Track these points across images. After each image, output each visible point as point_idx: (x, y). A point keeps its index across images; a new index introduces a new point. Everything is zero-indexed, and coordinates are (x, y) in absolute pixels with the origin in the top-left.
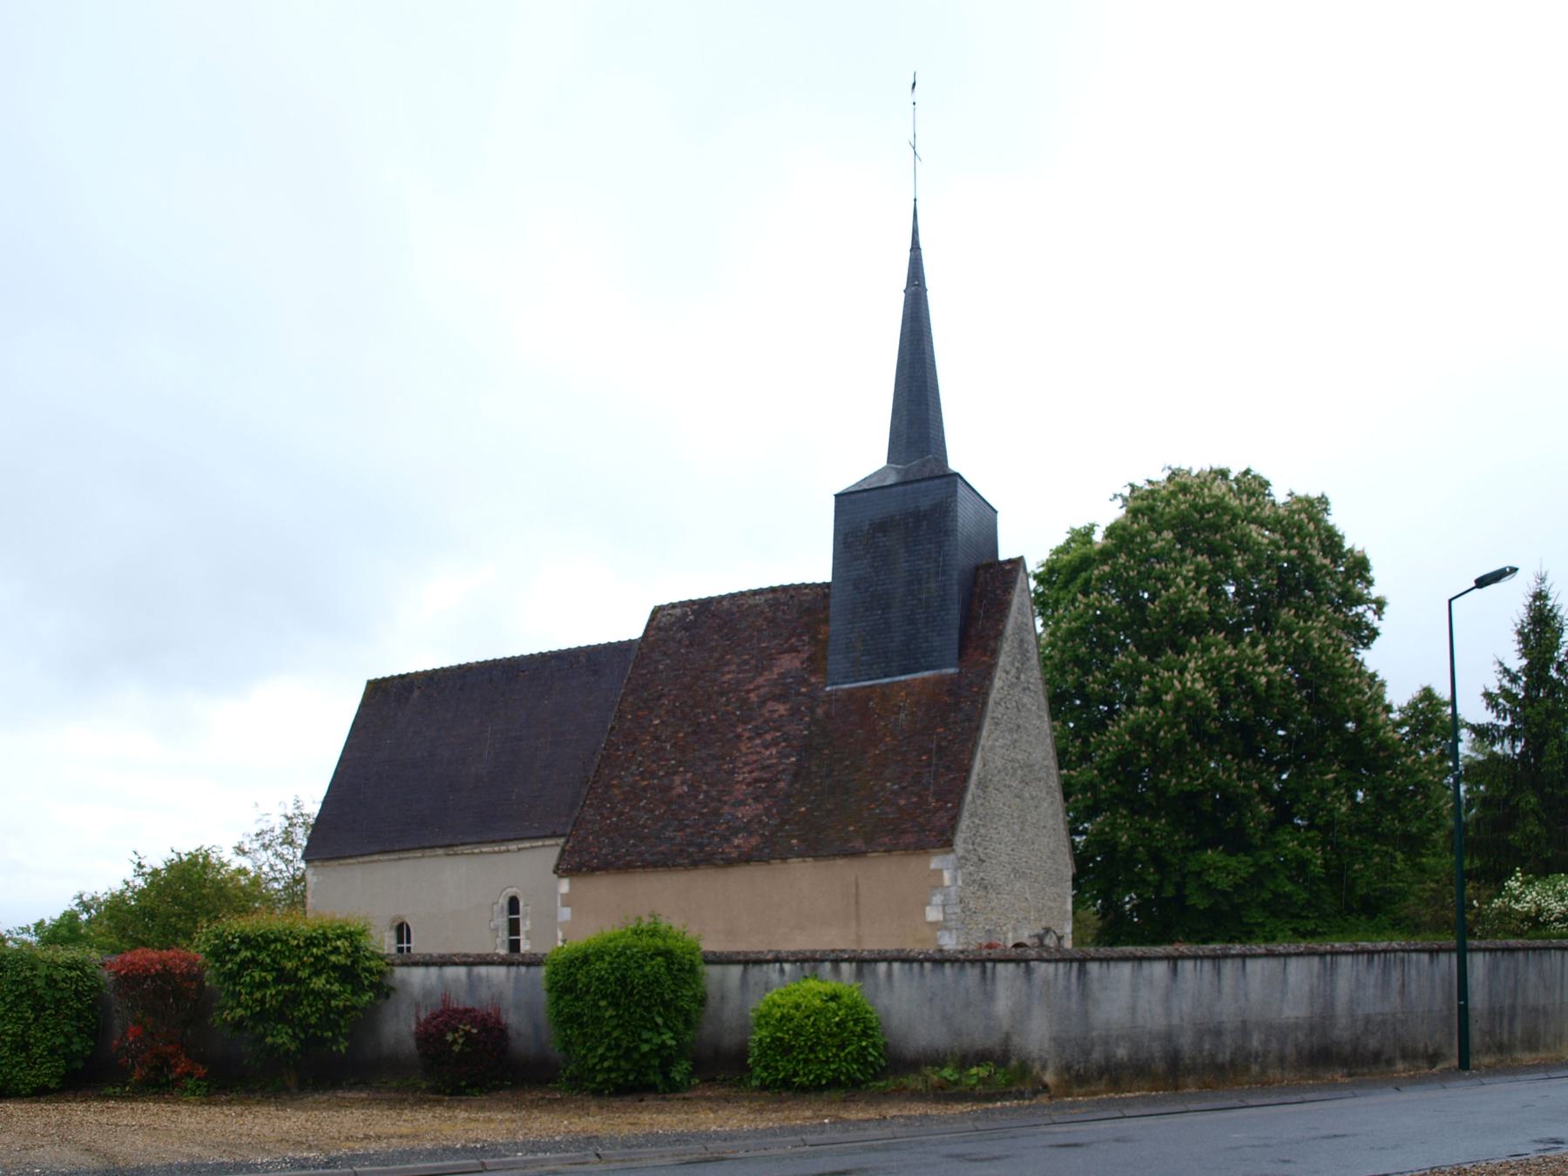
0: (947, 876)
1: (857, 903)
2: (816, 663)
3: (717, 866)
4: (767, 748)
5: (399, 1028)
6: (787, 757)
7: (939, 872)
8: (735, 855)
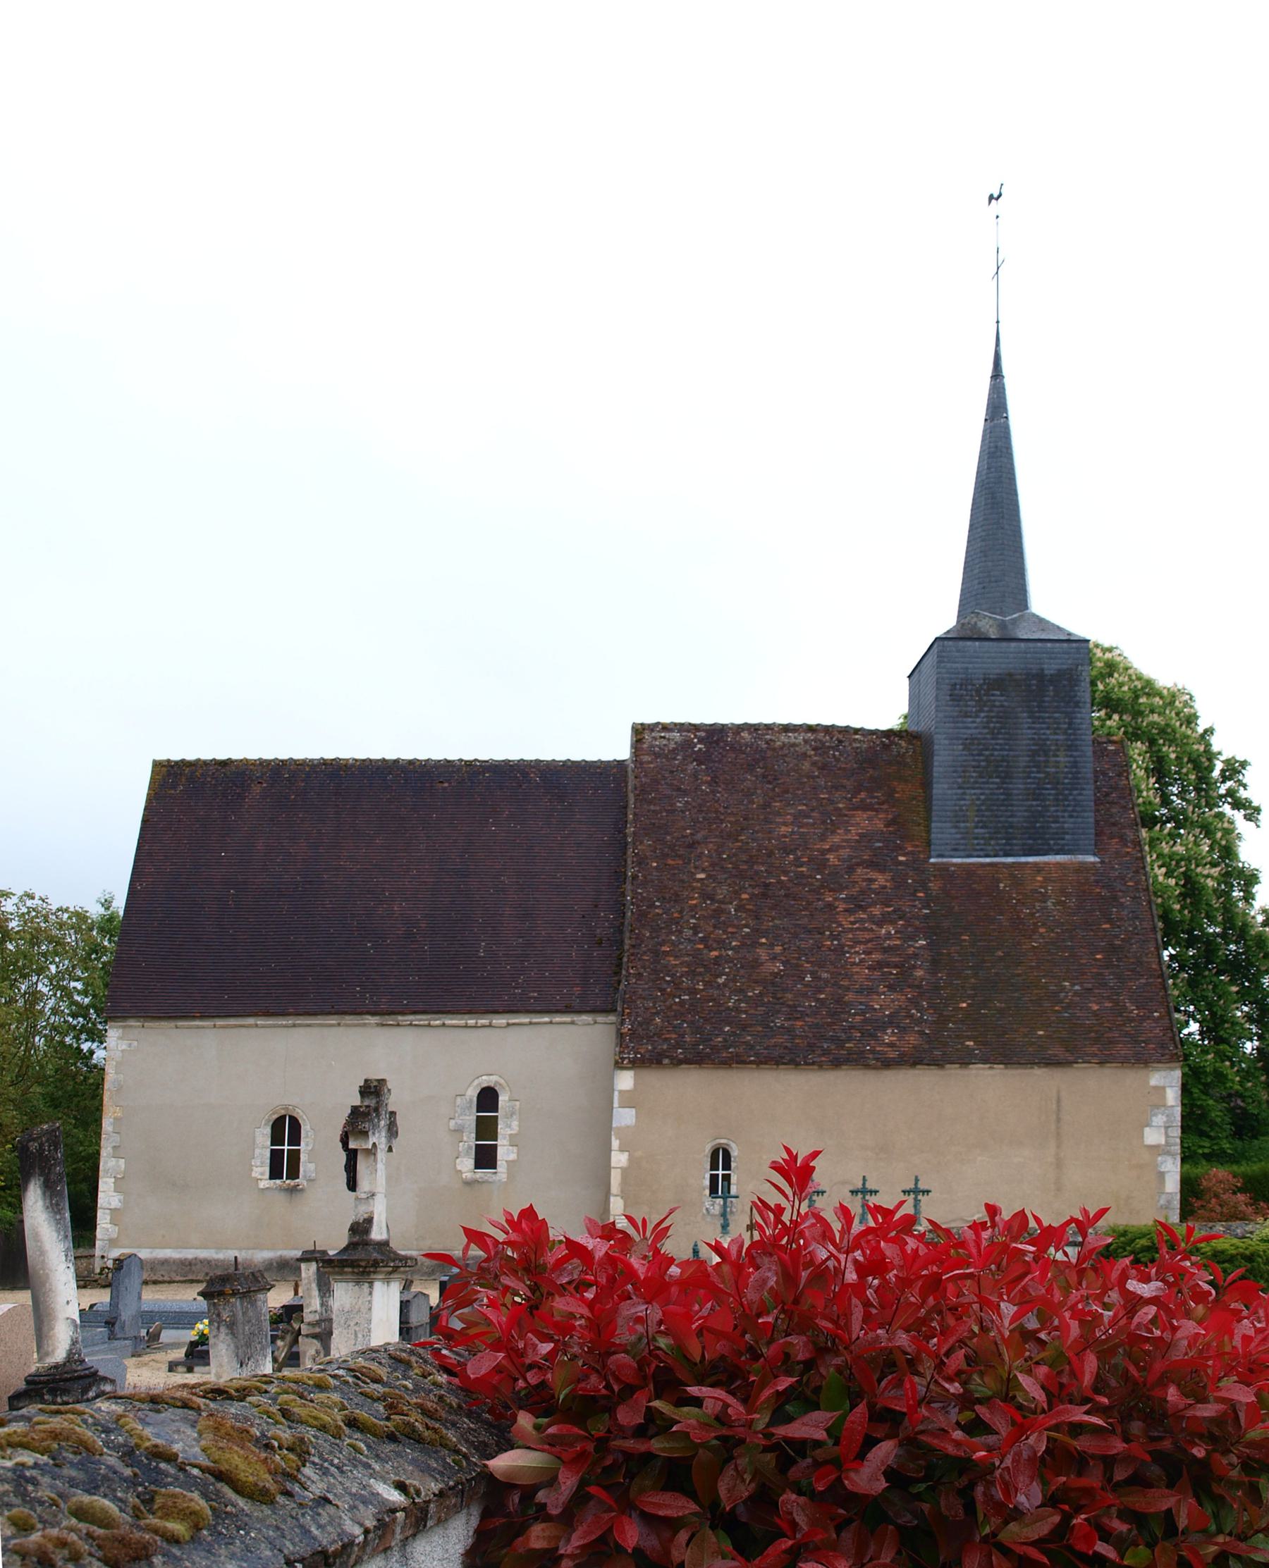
1: (1058, 1120)
3: (867, 1067)
4: (880, 924)
6: (913, 938)
7: (1161, 1090)
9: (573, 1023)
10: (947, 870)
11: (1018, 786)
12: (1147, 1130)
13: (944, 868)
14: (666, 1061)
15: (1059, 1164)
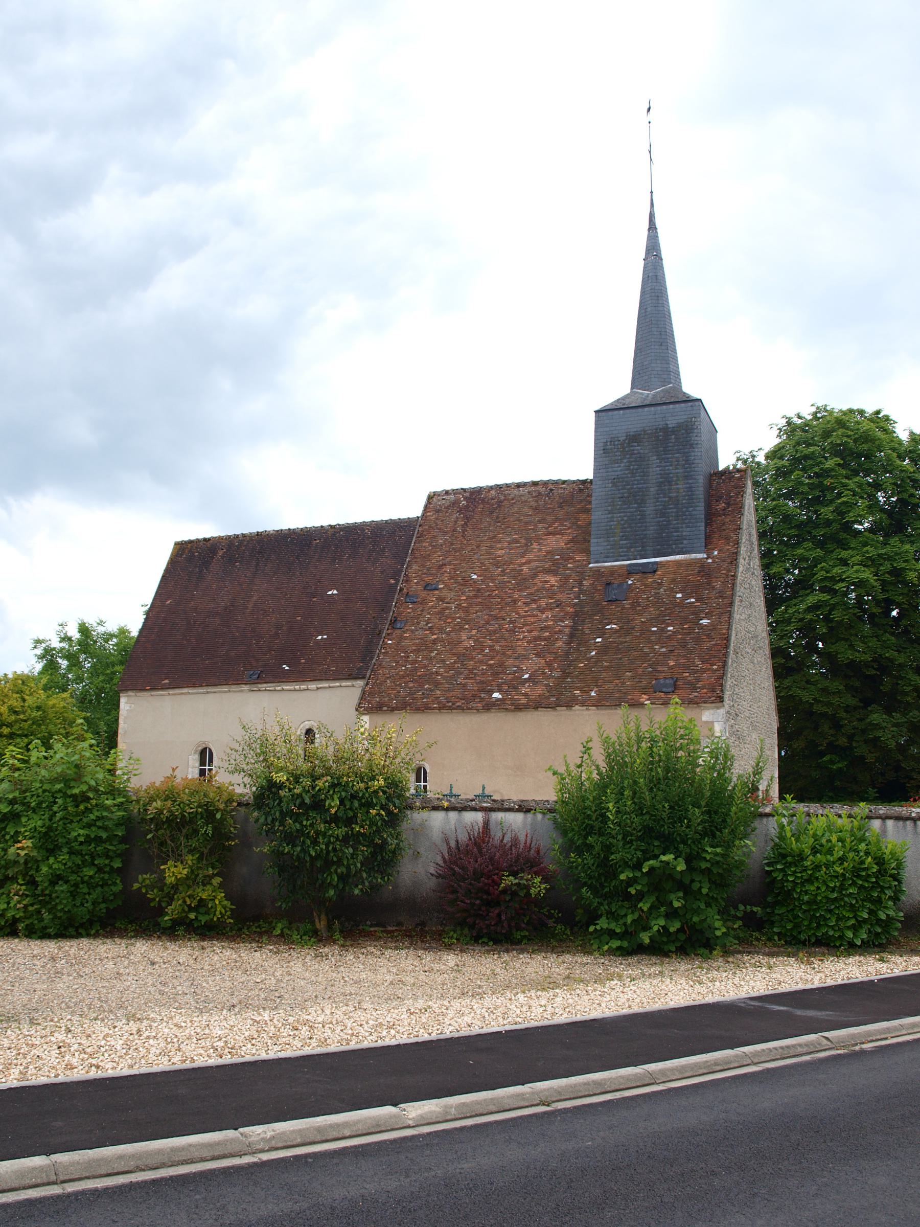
2: (582, 541)
5: (419, 870)
8: (524, 701)
9: (353, 686)
10: (599, 571)
11: (649, 508)
13: (597, 571)
14: (385, 708)
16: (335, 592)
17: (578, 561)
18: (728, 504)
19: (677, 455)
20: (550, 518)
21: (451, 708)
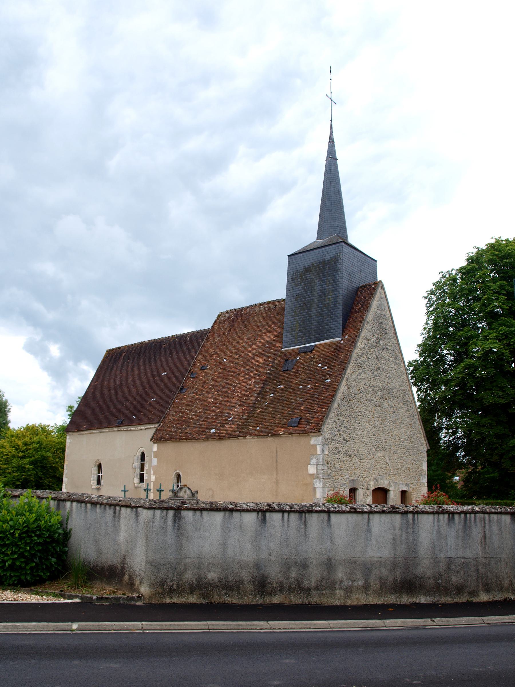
0: (319, 449)
1: (277, 462)
11: (314, 312)
12: (309, 466)
15: (277, 482)
16: (165, 373)
17: (277, 347)
18: (362, 305)
19: (329, 277)
20: (270, 323)
21: (191, 439)
